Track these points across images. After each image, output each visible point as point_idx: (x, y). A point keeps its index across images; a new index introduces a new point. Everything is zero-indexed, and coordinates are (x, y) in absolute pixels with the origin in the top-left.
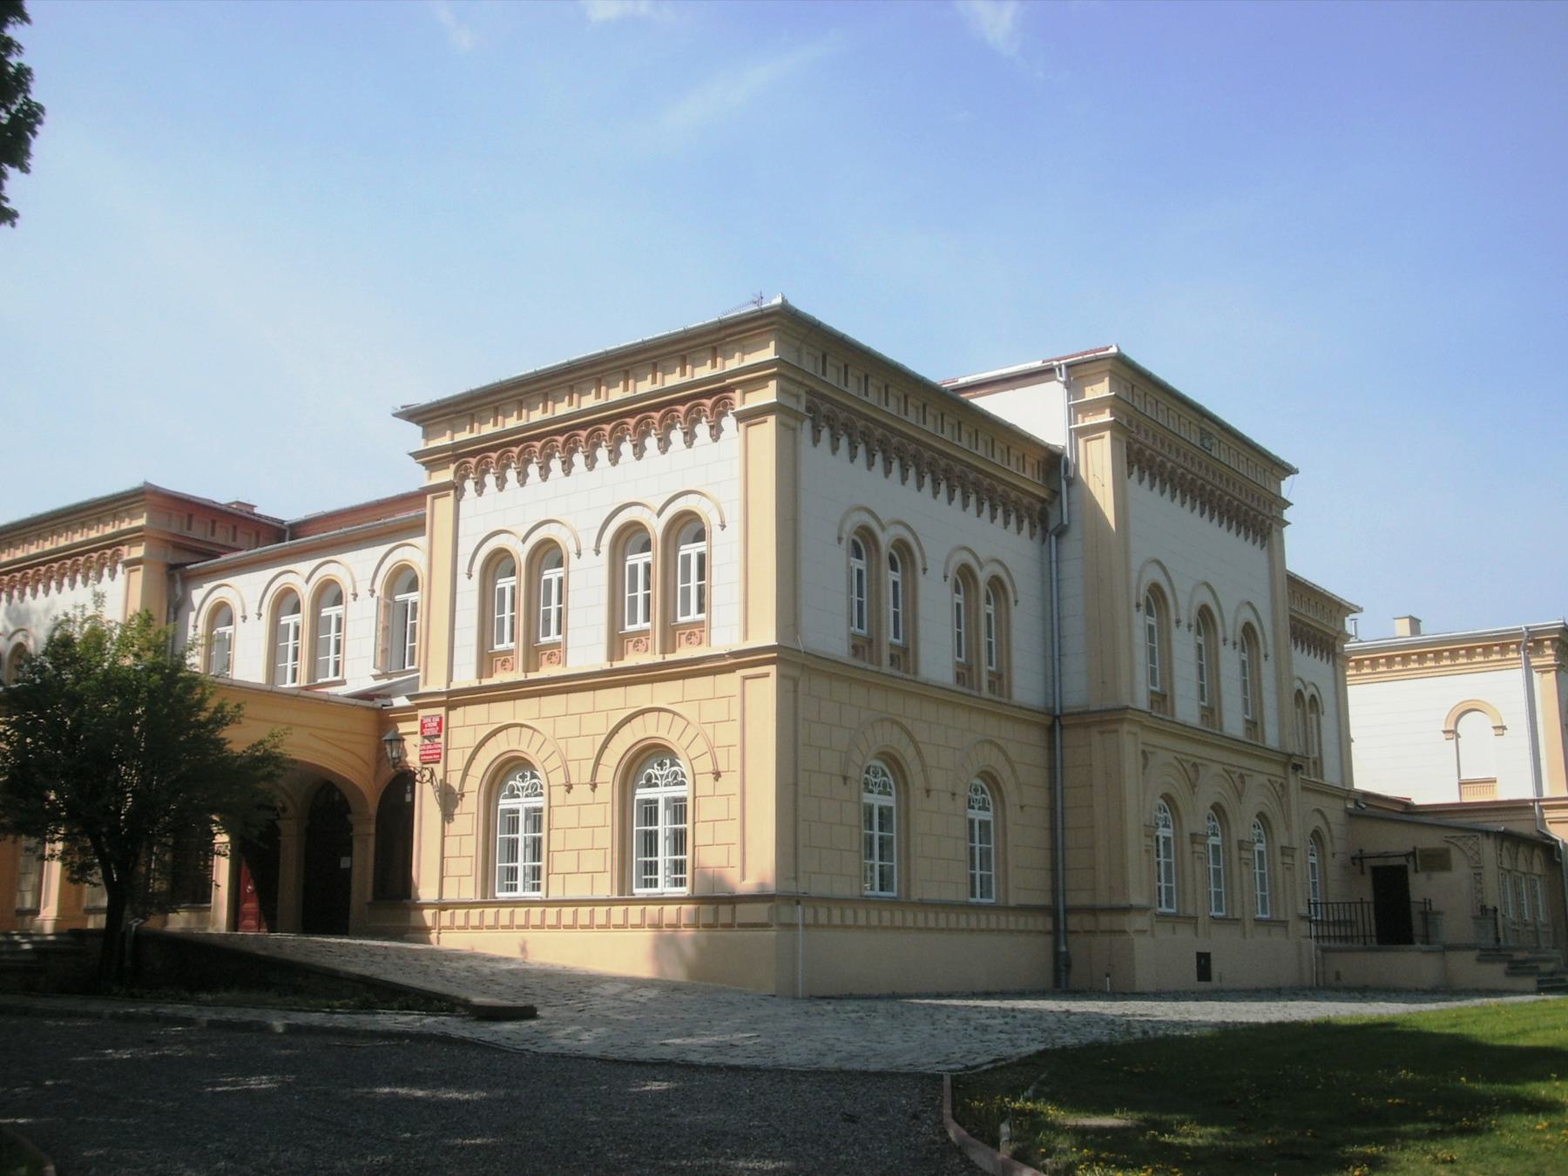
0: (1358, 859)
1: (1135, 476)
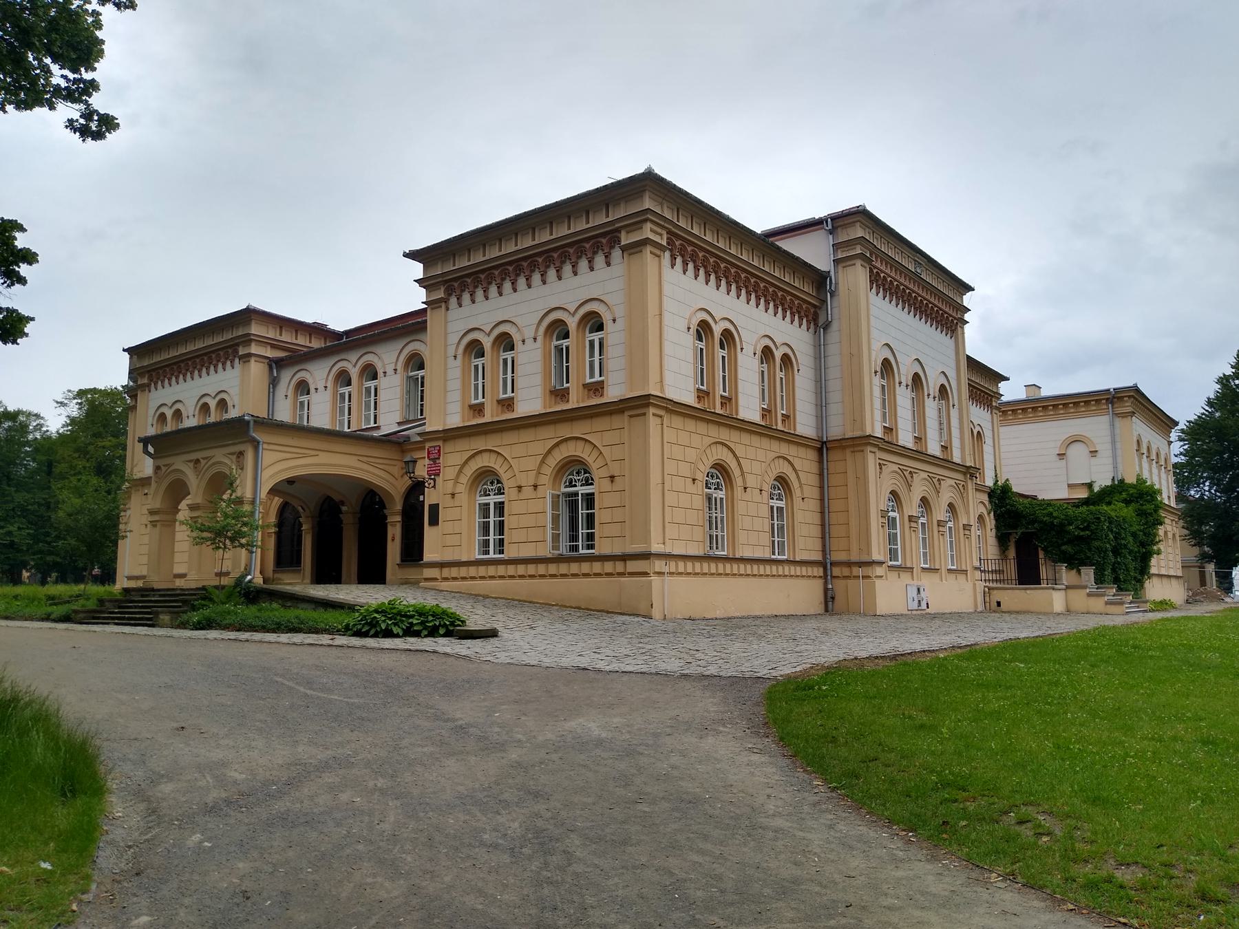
1: (874, 290)
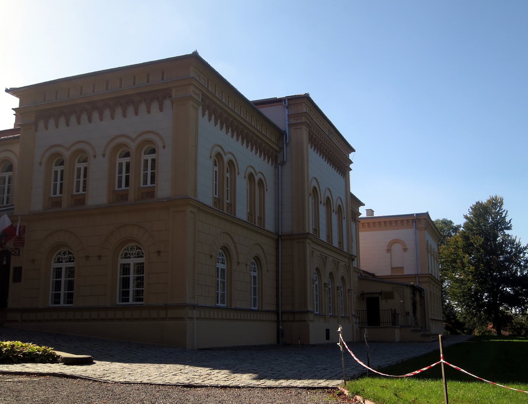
0: (362, 294)
